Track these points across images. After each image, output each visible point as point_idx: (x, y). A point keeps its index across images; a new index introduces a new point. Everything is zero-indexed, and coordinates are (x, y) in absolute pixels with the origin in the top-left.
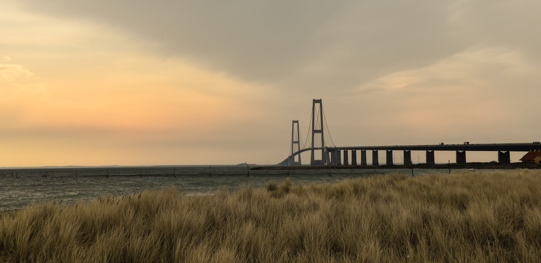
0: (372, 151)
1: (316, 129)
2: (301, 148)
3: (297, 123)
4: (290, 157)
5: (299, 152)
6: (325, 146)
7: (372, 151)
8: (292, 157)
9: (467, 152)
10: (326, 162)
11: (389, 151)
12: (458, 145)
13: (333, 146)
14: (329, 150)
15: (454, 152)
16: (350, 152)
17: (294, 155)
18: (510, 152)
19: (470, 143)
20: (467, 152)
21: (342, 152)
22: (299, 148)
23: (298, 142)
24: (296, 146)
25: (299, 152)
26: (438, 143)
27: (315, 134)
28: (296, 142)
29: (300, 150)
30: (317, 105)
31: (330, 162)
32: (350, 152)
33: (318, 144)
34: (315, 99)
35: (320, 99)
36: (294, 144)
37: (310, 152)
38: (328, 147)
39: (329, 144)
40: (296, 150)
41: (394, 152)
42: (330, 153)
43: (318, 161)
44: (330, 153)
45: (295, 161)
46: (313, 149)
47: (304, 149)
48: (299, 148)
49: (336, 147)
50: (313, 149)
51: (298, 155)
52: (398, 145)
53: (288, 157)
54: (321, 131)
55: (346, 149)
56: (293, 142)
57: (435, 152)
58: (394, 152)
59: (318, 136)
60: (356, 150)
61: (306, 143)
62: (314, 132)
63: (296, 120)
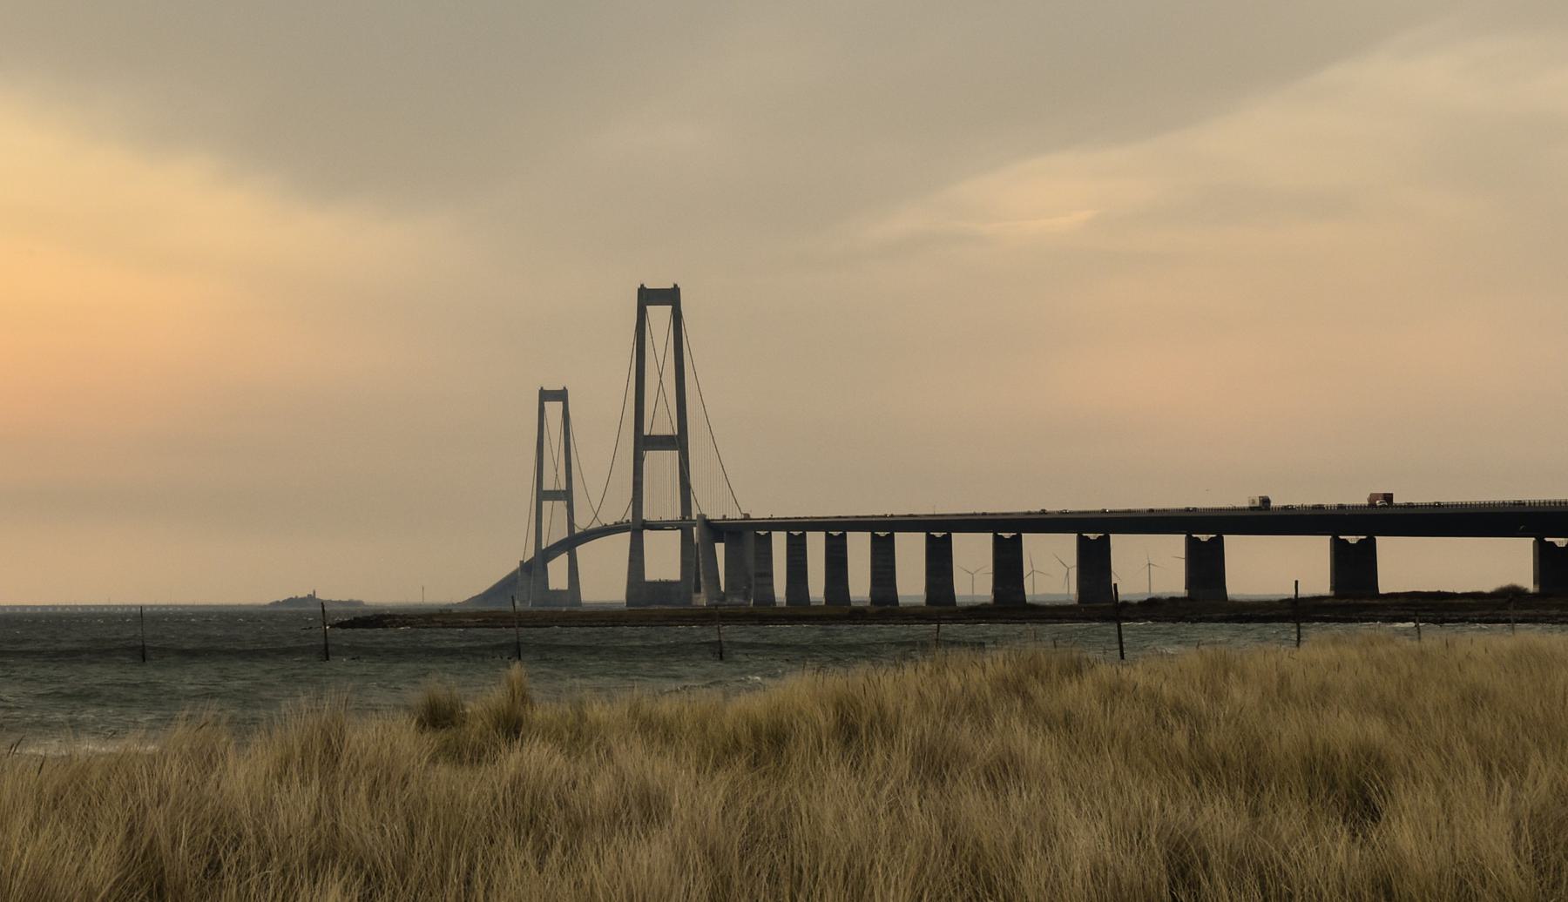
0: (991, 535)
1: (655, 432)
2: (583, 522)
4: (526, 567)
7: (991, 535)
8: (534, 568)
10: (702, 590)
11: (1007, 535)
12: (1341, 507)
13: (734, 514)
14: (717, 530)
15: (988, 537)
16: (816, 544)
17: (544, 556)
18: (1377, 538)
19: (1396, 501)
20: (1381, 541)
21: (779, 541)
23: (566, 495)
24: (554, 512)
26: (1240, 498)
27: (651, 457)
28: (554, 495)
29: (577, 531)
30: (659, 315)
31: (723, 589)
32: (816, 544)
33: (662, 502)
34: (545, 388)
35: (562, 388)
36: (547, 505)
37: (625, 537)
38: (709, 517)
39: (712, 505)
40: (555, 532)
42: (720, 548)
43: (663, 589)
44: (720, 548)
46: (637, 527)
47: (591, 527)
49: (747, 516)
50: (637, 527)
51: (563, 559)
52: (1048, 510)
53: (515, 565)
54: (678, 442)
55: (797, 530)
56: (542, 495)
59: (661, 464)
60: (773, 533)
63: (553, 385)
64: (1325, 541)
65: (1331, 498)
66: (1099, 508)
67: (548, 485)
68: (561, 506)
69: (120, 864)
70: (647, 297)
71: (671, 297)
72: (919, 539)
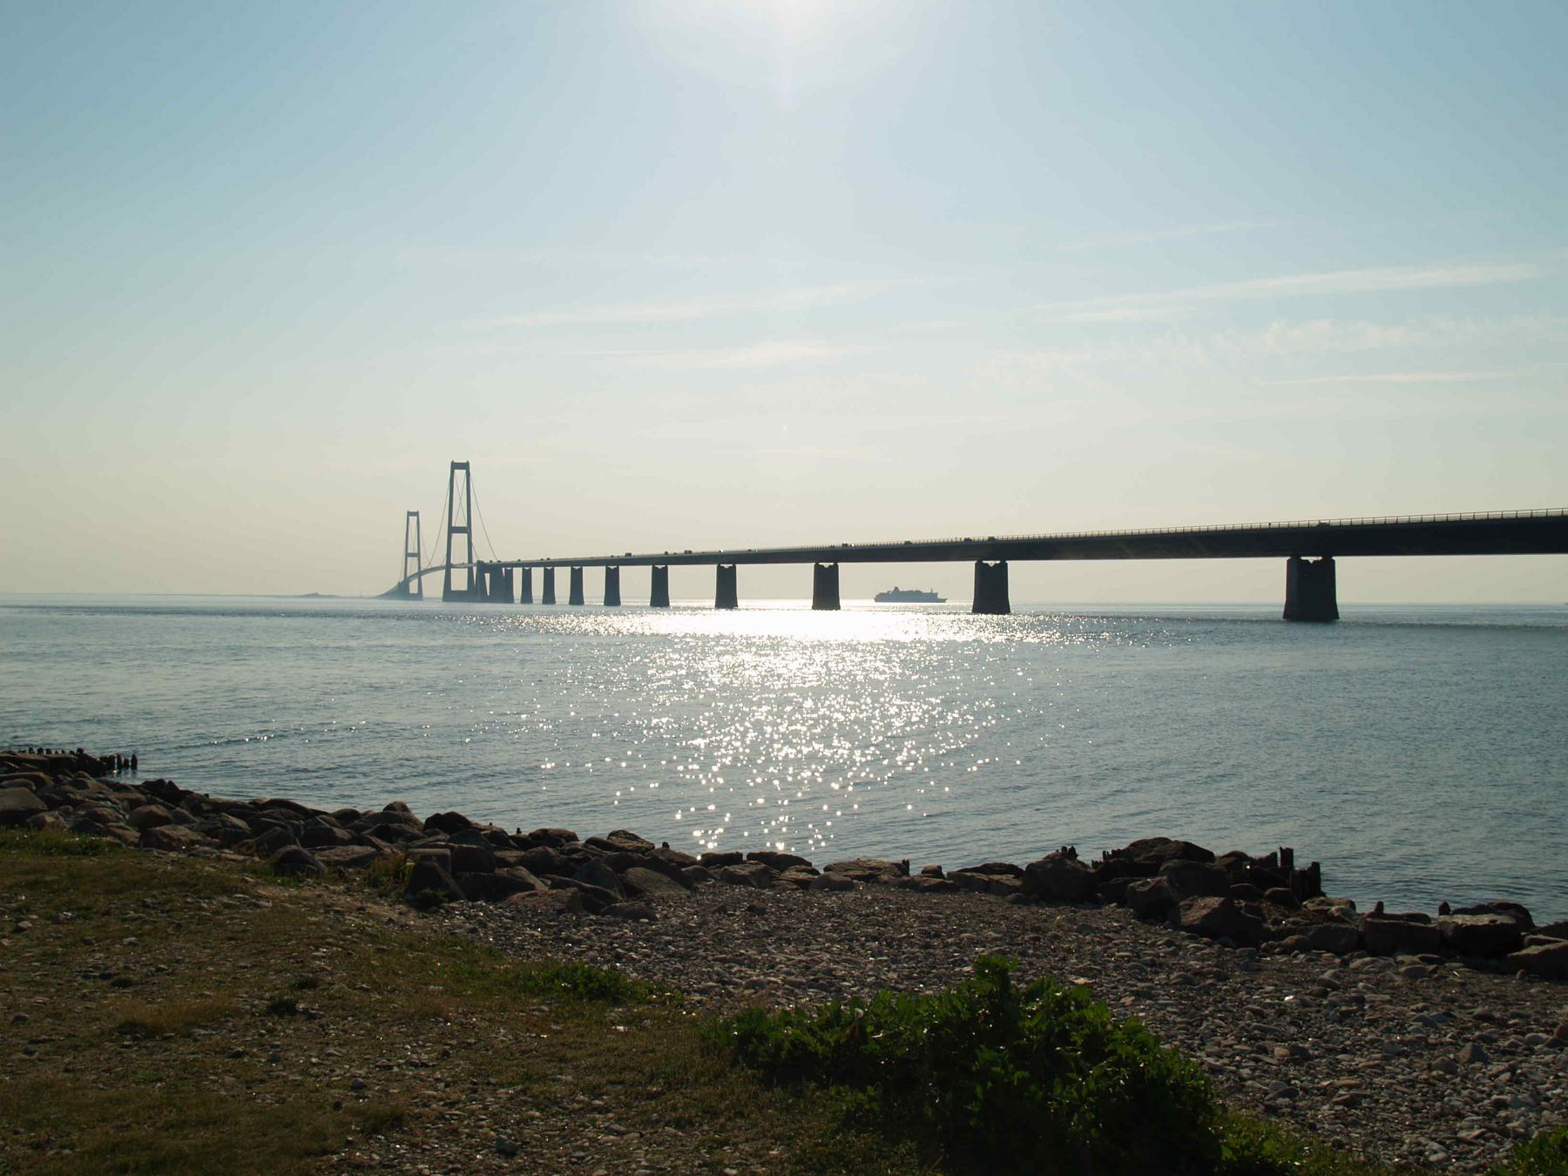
2: (424, 566)
3: (466, 535)
5: (419, 574)
6: (475, 561)
9: (584, 568)
11: (726, 566)
12: (908, 543)
14: (483, 567)
15: (569, 568)
16: (538, 574)
18: (1334, 558)
20: (584, 568)
21: (518, 574)
22: (419, 567)
23: (418, 555)
24: (413, 561)
25: (419, 574)
26: (620, 553)
27: (455, 536)
28: (413, 555)
30: (460, 474)
32: (538, 574)
33: (460, 556)
36: (409, 559)
39: (484, 555)
40: (413, 569)
41: (624, 571)
42: (487, 576)
44: (487, 576)
45: (453, 589)
46: (449, 567)
48: (419, 567)
52: (693, 551)
54: (467, 530)
55: (527, 567)
57: (671, 569)
58: (624, 571)
59: (460, 540)
61: (433, 554)
62: (452, 530)
64: (604, 568)
65: (980, 533)
66: (748, 548)
67: (410, 551)
68: (416, 559)
69: (1373, 637)
70: (455, 466)
71: (465, 466)
72: (541, 569)
